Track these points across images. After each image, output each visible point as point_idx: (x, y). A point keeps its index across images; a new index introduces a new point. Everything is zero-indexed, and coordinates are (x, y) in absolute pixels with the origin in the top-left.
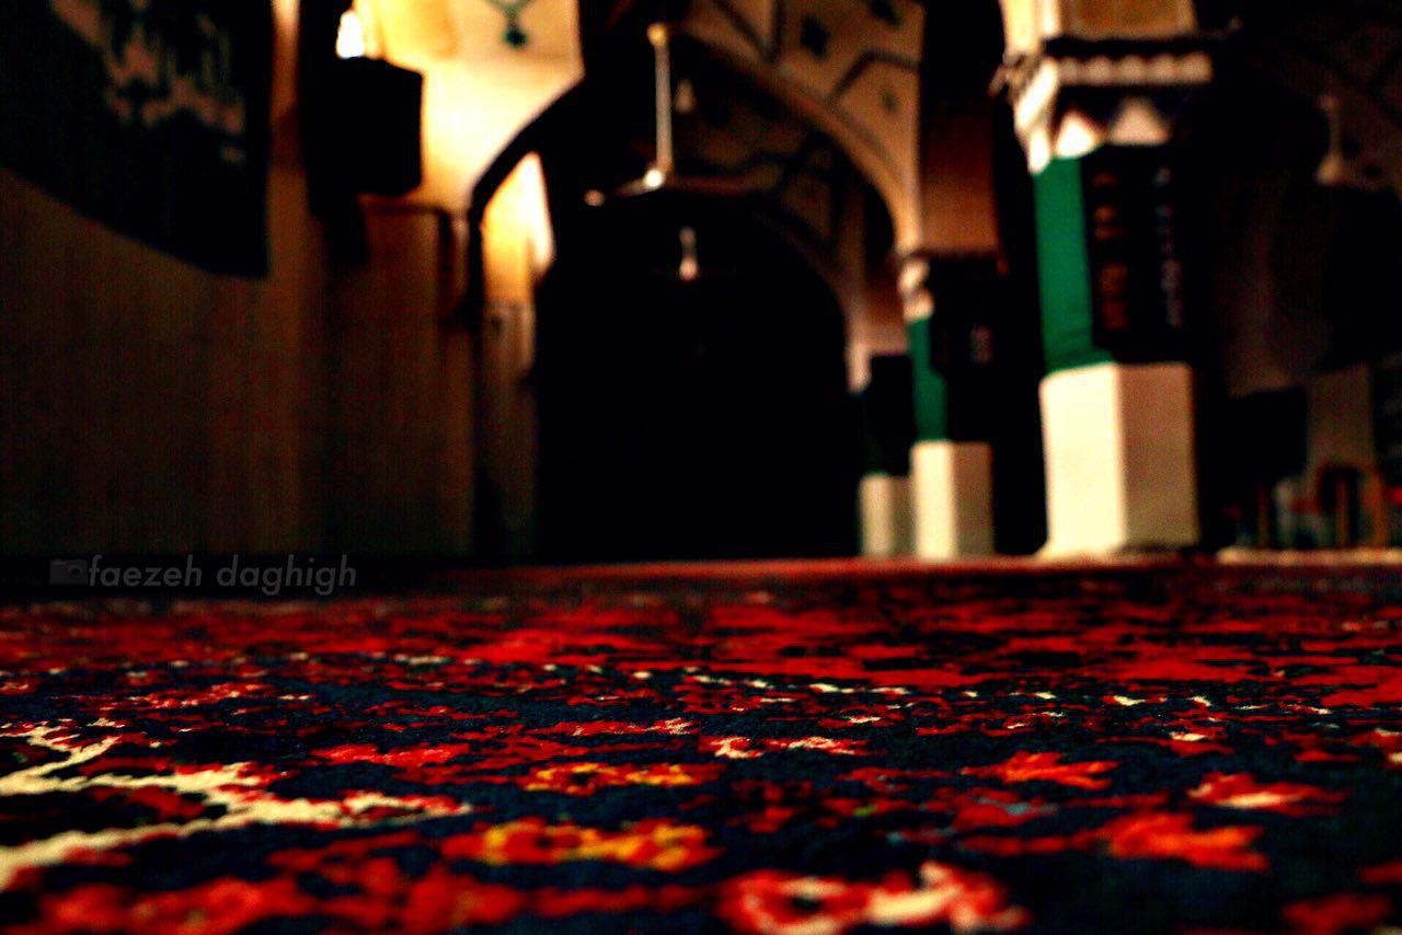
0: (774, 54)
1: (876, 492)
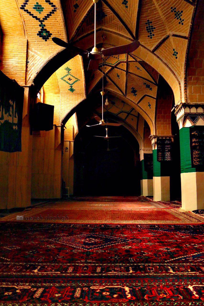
0: (125, 95)
1: (145, 182)
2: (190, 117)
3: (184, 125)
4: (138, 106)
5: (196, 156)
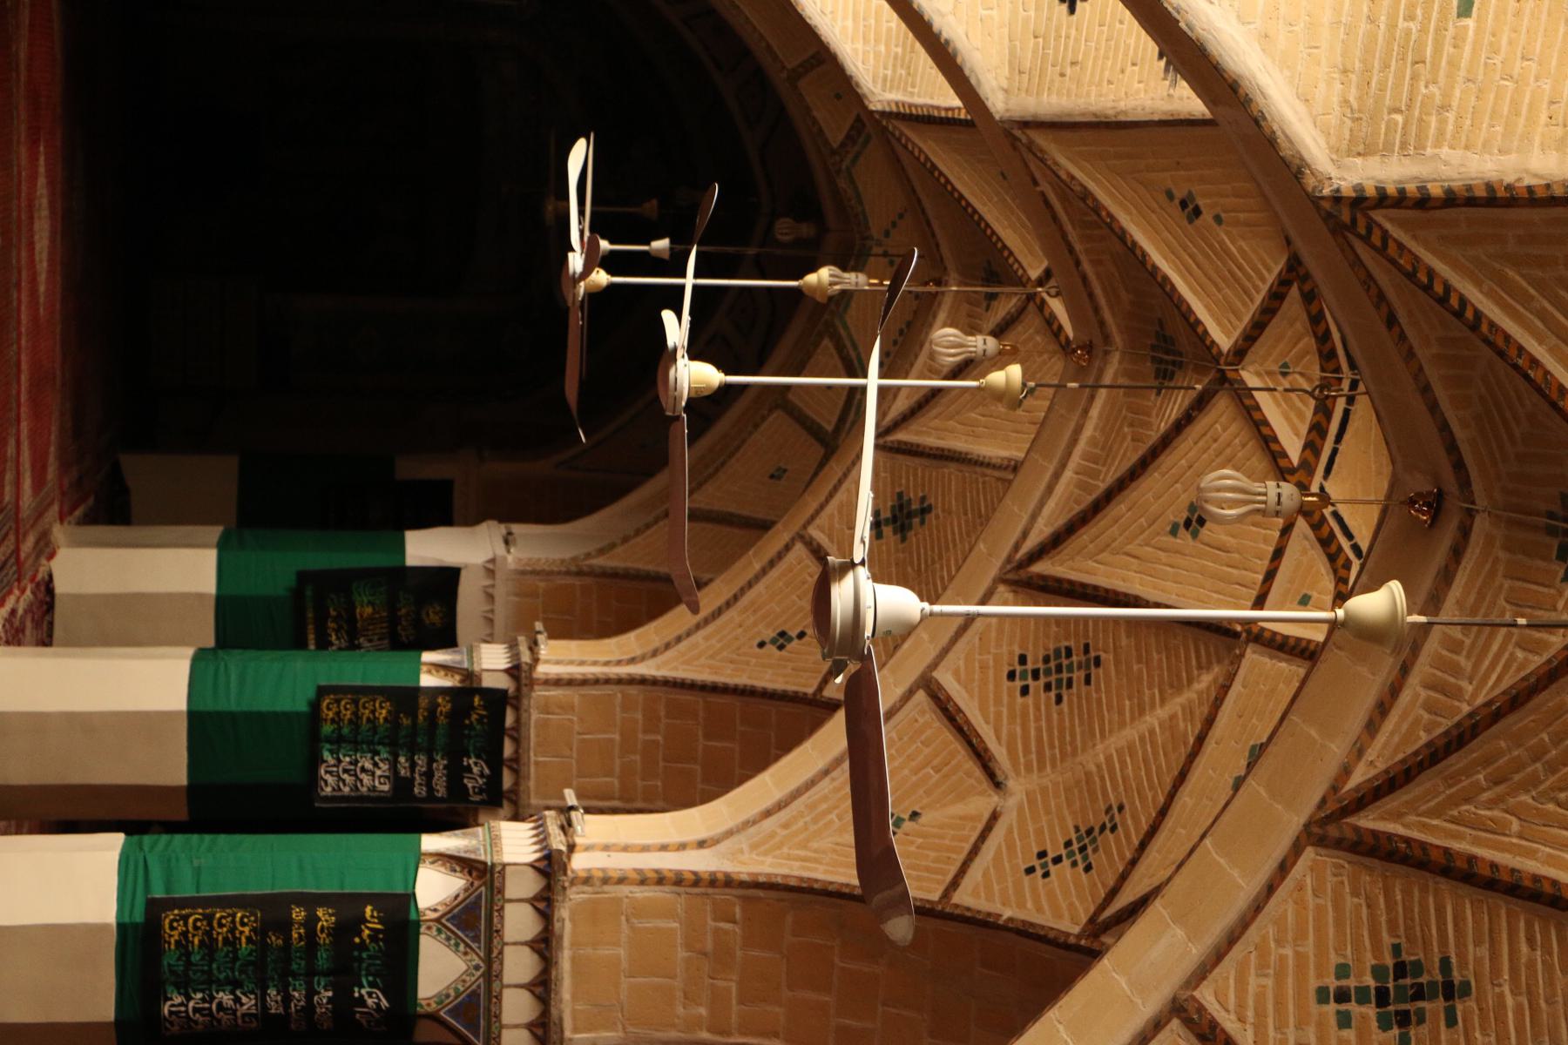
2: (480, 896)
3: (433, 863)
4: (787, 548)
5: (221, 925)
